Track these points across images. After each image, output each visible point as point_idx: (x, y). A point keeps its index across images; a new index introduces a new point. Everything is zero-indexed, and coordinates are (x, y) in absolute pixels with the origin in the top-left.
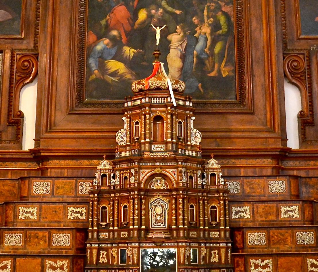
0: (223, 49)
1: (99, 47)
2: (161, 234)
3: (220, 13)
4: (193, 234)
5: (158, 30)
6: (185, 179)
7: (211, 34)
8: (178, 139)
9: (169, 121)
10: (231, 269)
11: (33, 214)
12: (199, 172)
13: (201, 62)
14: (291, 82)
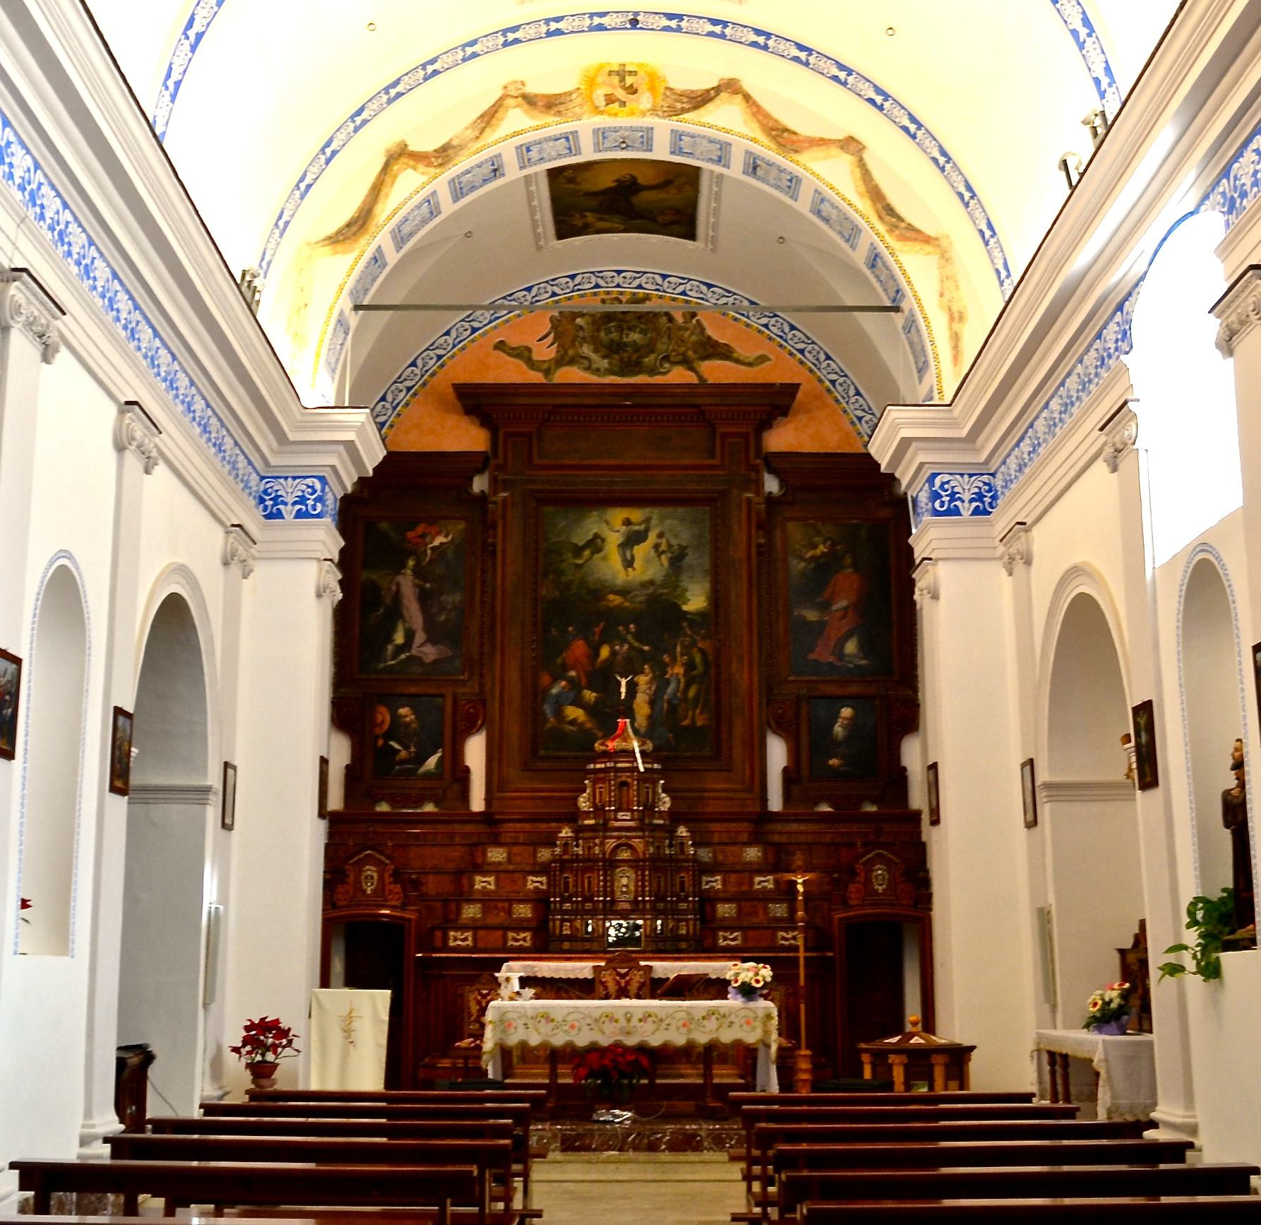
0: (698, 693)
1: (554, 691)
2: (626, 906)
3: (696, 650)
4: (661, 906)
5: (624, 682)
6: (651, 850)
7: (685, 674)
8: (645, 806)
9: (635, 788)
10: (315, 512)
11: (490, 884)
12: (667, 842)
13: (673, 708)
14: (774, 732)
